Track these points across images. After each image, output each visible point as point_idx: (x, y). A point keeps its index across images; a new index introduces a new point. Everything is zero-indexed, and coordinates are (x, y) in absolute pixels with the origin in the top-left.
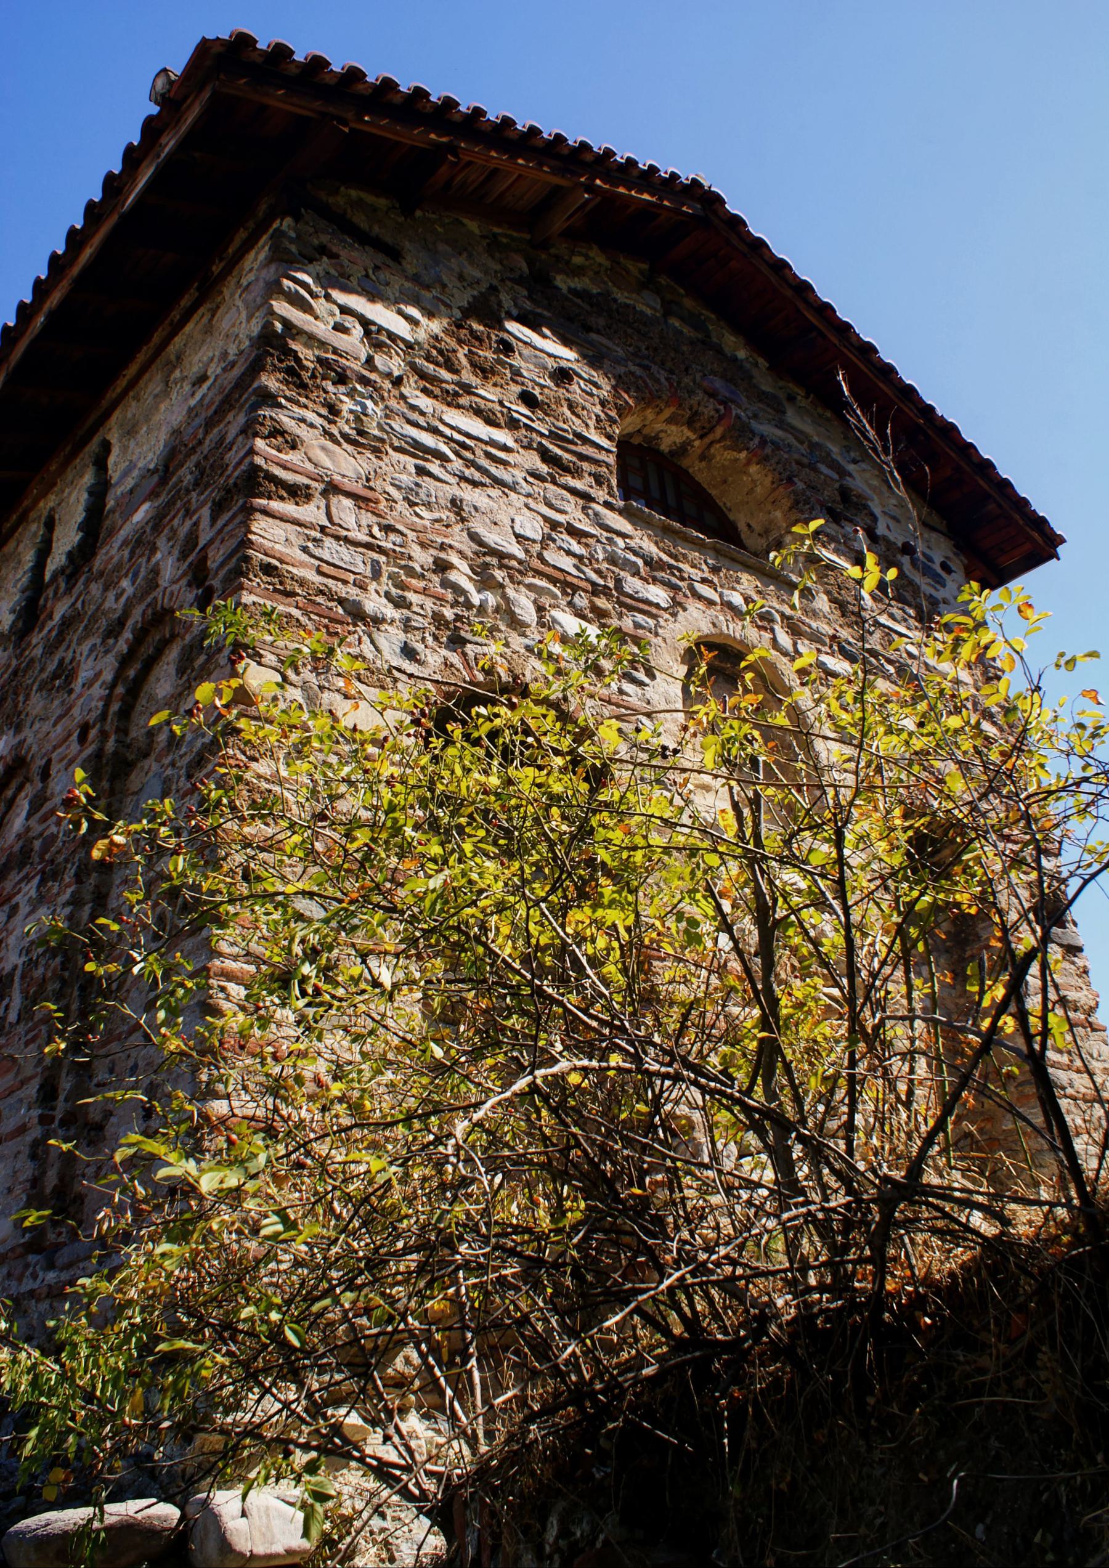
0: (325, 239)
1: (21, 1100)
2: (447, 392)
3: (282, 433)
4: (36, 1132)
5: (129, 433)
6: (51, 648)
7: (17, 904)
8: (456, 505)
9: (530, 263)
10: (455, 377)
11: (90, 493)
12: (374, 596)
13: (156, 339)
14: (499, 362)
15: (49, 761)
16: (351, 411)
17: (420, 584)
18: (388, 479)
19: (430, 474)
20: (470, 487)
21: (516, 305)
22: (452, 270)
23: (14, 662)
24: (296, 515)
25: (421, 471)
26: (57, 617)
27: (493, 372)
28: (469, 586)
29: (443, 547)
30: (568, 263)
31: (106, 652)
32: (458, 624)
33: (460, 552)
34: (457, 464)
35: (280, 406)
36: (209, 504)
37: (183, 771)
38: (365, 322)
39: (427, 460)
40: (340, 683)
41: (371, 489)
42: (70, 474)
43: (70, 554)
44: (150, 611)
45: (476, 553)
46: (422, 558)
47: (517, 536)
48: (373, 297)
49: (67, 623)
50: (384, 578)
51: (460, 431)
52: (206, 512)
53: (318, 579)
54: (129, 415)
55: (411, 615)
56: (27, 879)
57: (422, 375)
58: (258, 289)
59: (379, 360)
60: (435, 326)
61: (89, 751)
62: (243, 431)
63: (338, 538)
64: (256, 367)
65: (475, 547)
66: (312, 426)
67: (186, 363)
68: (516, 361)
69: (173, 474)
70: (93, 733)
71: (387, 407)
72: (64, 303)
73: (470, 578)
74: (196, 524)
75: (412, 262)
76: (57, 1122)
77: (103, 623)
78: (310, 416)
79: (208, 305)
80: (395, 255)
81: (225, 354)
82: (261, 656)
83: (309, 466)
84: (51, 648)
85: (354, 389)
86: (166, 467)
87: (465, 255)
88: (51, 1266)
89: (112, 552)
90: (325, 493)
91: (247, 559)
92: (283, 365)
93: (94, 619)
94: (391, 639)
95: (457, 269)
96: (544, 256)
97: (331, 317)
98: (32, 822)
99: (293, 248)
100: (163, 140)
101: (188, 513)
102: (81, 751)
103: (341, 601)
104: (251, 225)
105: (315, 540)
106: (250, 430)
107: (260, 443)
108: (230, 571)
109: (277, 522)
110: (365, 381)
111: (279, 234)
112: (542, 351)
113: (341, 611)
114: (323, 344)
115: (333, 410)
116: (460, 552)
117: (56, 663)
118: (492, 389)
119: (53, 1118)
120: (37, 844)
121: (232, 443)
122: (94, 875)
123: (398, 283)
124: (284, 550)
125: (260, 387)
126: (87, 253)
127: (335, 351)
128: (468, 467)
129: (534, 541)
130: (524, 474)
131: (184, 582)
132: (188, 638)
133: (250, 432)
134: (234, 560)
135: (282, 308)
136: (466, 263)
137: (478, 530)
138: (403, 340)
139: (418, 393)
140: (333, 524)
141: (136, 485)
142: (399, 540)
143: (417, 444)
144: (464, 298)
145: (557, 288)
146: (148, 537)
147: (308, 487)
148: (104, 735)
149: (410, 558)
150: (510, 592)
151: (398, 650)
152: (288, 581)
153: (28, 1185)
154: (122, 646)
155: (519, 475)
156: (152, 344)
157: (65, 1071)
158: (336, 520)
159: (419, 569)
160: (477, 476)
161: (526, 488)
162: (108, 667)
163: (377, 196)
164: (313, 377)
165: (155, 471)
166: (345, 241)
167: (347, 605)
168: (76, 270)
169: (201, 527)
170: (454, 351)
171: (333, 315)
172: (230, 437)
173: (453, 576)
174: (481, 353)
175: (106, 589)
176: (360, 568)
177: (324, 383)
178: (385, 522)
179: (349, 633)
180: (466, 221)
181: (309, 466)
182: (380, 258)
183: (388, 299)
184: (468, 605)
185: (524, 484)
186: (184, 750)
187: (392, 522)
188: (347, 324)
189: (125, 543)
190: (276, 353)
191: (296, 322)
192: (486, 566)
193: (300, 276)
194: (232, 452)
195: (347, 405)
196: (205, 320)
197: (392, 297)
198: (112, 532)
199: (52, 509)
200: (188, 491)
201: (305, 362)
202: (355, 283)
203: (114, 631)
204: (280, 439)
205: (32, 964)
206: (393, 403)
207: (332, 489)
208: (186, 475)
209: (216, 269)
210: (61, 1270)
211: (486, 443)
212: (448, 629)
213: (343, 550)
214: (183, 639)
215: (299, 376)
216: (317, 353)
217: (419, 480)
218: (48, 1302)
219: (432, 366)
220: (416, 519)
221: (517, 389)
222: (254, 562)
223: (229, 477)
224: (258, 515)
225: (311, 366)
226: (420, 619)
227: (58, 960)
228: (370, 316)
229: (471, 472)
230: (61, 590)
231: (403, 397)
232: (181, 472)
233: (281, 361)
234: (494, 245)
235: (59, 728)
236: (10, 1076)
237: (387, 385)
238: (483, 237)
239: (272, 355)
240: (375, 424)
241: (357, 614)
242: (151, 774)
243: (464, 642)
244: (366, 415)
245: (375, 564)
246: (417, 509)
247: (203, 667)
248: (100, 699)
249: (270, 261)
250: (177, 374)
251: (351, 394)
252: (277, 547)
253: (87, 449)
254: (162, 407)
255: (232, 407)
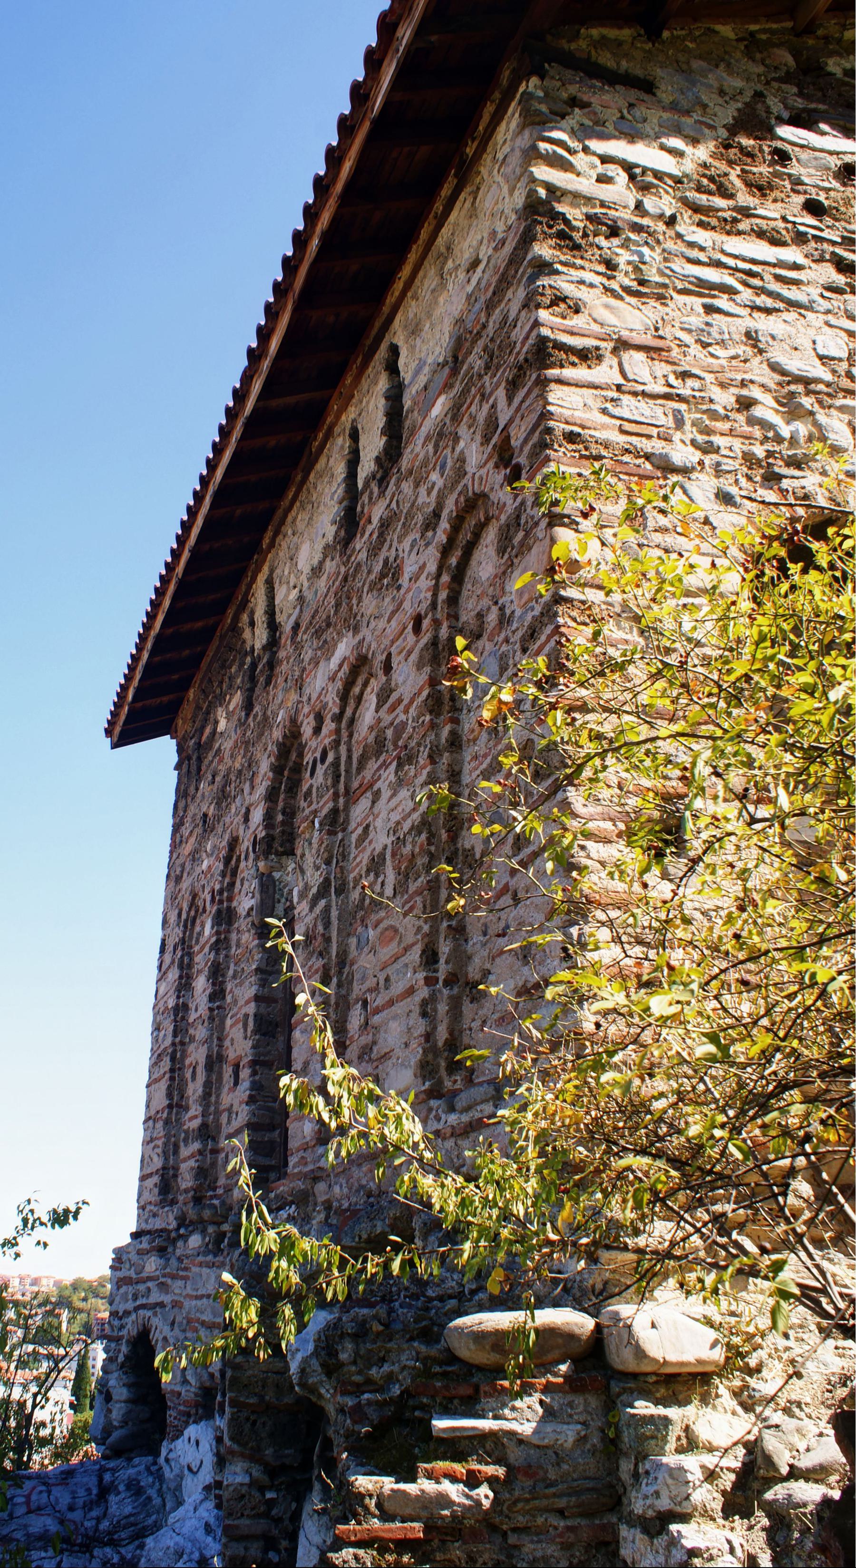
0: (573, 89)
1: (406, 965)
2: (725, 220)
3: (564, 299)
4: (424, 992)
5: (413, 333)
6: (374, 551)
7: (379, 790)
8: (751, 337)
9: (796, 56)
10: (731, 203)
11: (387, 398)
12: (680, 445)
13: (424, 234)
14: (776, 174)
15: (389, 655)
16: (629, 263)
17: (725, 426)
18: (677, 325)
19: (719, 311)
20: (763, 316)
21: (786, 107)
22: (711, 86)
23: (343, 570)
24: (590, 379)
25: (710, 309)
26: (375, 520)
27: (771, 188)
28: (776, 419)
29: (743, 384)
30: (839, 41)
31: (427, 545)
32: (771, 461)
33: (763, 386)
34: (746, 295)
35: (557, 272)
36: (503, 384)
37: (518, 646)
38: (628, 167)
39: (714, 297)
40: (657, 538)
41: (661, 337)
42: (365, 384)
43: (378, 460)
44: (462, 499)
45: (780, 384)
46: (724, 399)
47: (821, 358)
48: (632, 137)
49: (385, 525)
50: (688, 427)
51: (744, 260)
52: (501, 393)
53: (622, 439)
54: (411, 315)
55: (720, 459)
56: (385, 765)
57: (696, 209)
58: (515, 160)
59: (650, 203)
60: (702, 153)
61: (425, 639)
62: (525, 306)
63: (635, 394)
64: (527, 239)
65: (778, 378)
66: (591, 286)
67: (456, 251)
68: (794, 169)
69: (463, 362)
70: (426, 623)
71: (664, 250)
72: (335, 221)
73: (777, 411)
74: (493, 406)
75: (666, 92)
76: (441, 982)
77: (419, 518)
78: (589, 277)
79: (468, 189)
80: (647, 87)
81: (494, 233)
82: (577, 524)
83: (596, 328)
84: (374, 551)
85: (628, 239)
86: (455, 358)
87: (722, 66)
88: (452, 1109)
89: (416, 449)
90: (615, 351)
91: (549, 431)
92: (554, 230)
93: (410, 515)
94: (703, 487)
95: (716, 85)
96: (811, 42)
97: (593, 168)
98: (382, 713)
99: (544, 108)
100: (399, 33)
101: (484, 397)
102: (417, 641)
103: (648, 457)
104: (497, 95)
105: (612, 400)
106: (531, 303)
107: (543, 315)
108: (534, 446)
109: (573, 389)
110: (637, 228)
111: (528, 97)
112: (822, 151)
113: (648, 466)
114: (589, 200)
115: (610, 265)
116: (763, 386)
117: (381, 563)
118: (772, 206)
119: (437, 979)
120: (389, 733)
121: (516, 320)
122: (446, 754)
123: (655, 116)
124: (583, 415)
125: (534, 258)
126: (347, 167)
127: (603, 205)
128: (758, 295)
129: (840, 360)
130: (819, 290)
131: (491, 464)
132: (503, 518)
133: (532, 305)
134: (537, 434)
135: (543, 172)
136: (724, 75)
137: (778, 359)
138: (670, 176)
139: (694, 228)
140: (628, 380)
141: (430, 381)
142: (697, 384)
143: (701, 283)
144: (727, 114)
145: (830, 74)
146: (449, 428)
147: (597, 348)
148: (437, 623)
149: (711, 401)
150: (821, 417)
151: (712, 497)
152: (593, 446)
153: (422, 1040)
154: (441, 537)
155: (814, 292)
156: (420, 242)
157: (442, 936)
158: (631, 376)
159: (722, 411)
160: (769, 302)
161: (824, 305)
162: (431, 558)
163: (620, 28)
164: (585, 235)
165: (445, 363)
166: (594, 87)
167: (653, 459)
168: (339, 187)
169: (499, 408)
170: (726, 175)
171: (594, 167)
172: (512, 315)
173: (758, 412)
174: (755, 170)
175: (417, 485)
176: (662, 420)
177: (597, 240)
178: (680, 369)
179: (661, 487)
180: (718, 27)
181: (596, 328)
182: (633, 94)
183: (648, 136)
184: (779, 439)
185: (820, 300)
186: (515, 625)
187: (687, 368)
188: (610, 174)
189: (428, 438)
190: (545, 220)
191: (558, 184)
192: (792, 395)
193: (556, 135)
194: (518, 328)
195: (623, 257)
196: (468, 205)
197: (652, 133)
198: (413, 431)
199: (354, 421)
200: (480, 376)
201: (574, 223)
202: (611, 128)
203: (431, 522)
204: (562, 306)
205: (400, 842)
206: (670, 245)
207: (622, 345)
208: (475, 361)
209: (470, 151)
210: (461, 1112)
211: (774, 266)
212: (761, 467)
213: (642, 404)
214: (498, 519)
215: (571, 238)
216: (584, 210)
217: (709, 319)
218: (453, 1140)
219: (704, 197)
220: (711, 360)
221: (800, 199)
222: (557, 433)
223: (518, 353)
224: (553, 386)
225: (581, 225)
226: (730, 461)
227: (424, 836)
228: (631, 159)
229: (763, 301)
230: (375, 495)
231: (679, 236)
232: (471, 359)
233: (550, 227)
234: (753, 46)
235: (393, 623)
236: (394, 944)
237: (661, 227)
238: (738, 40)
239: (541, 223)
240: (654, 271)
241: (666, 467)
242: (486, 653)
243: (779, 477)
244: (644, 263)
245: (677, 413)
246: (710, 349)
247: (522, 544)
248: (428, 590)
249: (522, 127)
250: (450, 264)
251: (625, 245)
252: (577, 413)
253: (377, 357)
254: (441, 300)
255: (509, 284)
